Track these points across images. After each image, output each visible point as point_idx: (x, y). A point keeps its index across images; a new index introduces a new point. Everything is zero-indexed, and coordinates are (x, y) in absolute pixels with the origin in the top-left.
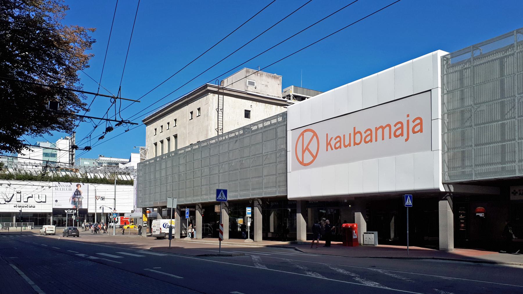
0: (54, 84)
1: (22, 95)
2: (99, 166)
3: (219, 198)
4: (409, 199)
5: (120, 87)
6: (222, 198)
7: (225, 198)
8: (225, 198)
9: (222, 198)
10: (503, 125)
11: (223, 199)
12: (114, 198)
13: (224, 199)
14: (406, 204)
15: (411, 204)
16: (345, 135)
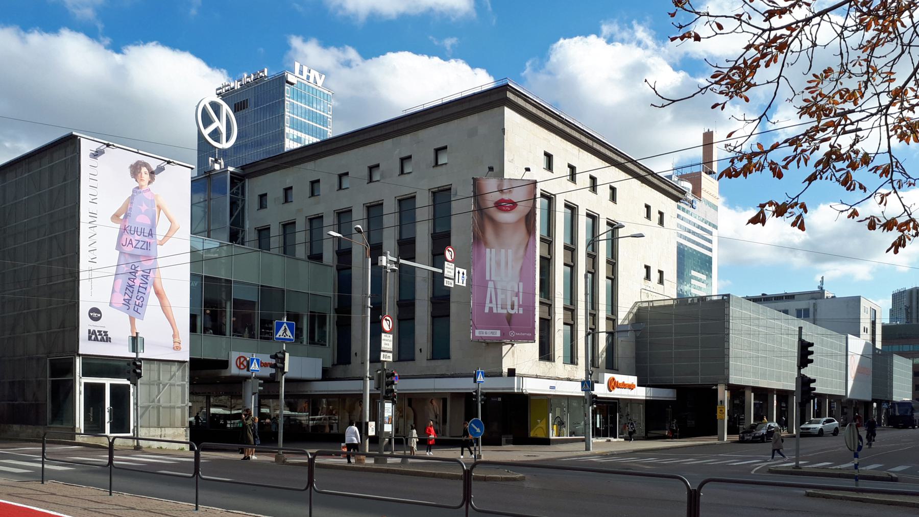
0: (915, 129)
1: (669, 408)
2: (825, 148)
3: (280, 336)
4: (285, 329)
5: (828, 44)
6: (285, 336)
7: (290, 336)
8: (290, 336)
9: (285, 336)
10: (65, 180)
11: (286, 337)
12: (169, 409)
13: (288, 337)
14: (277, 336)
15: (292, 338)
16: (802, 327)
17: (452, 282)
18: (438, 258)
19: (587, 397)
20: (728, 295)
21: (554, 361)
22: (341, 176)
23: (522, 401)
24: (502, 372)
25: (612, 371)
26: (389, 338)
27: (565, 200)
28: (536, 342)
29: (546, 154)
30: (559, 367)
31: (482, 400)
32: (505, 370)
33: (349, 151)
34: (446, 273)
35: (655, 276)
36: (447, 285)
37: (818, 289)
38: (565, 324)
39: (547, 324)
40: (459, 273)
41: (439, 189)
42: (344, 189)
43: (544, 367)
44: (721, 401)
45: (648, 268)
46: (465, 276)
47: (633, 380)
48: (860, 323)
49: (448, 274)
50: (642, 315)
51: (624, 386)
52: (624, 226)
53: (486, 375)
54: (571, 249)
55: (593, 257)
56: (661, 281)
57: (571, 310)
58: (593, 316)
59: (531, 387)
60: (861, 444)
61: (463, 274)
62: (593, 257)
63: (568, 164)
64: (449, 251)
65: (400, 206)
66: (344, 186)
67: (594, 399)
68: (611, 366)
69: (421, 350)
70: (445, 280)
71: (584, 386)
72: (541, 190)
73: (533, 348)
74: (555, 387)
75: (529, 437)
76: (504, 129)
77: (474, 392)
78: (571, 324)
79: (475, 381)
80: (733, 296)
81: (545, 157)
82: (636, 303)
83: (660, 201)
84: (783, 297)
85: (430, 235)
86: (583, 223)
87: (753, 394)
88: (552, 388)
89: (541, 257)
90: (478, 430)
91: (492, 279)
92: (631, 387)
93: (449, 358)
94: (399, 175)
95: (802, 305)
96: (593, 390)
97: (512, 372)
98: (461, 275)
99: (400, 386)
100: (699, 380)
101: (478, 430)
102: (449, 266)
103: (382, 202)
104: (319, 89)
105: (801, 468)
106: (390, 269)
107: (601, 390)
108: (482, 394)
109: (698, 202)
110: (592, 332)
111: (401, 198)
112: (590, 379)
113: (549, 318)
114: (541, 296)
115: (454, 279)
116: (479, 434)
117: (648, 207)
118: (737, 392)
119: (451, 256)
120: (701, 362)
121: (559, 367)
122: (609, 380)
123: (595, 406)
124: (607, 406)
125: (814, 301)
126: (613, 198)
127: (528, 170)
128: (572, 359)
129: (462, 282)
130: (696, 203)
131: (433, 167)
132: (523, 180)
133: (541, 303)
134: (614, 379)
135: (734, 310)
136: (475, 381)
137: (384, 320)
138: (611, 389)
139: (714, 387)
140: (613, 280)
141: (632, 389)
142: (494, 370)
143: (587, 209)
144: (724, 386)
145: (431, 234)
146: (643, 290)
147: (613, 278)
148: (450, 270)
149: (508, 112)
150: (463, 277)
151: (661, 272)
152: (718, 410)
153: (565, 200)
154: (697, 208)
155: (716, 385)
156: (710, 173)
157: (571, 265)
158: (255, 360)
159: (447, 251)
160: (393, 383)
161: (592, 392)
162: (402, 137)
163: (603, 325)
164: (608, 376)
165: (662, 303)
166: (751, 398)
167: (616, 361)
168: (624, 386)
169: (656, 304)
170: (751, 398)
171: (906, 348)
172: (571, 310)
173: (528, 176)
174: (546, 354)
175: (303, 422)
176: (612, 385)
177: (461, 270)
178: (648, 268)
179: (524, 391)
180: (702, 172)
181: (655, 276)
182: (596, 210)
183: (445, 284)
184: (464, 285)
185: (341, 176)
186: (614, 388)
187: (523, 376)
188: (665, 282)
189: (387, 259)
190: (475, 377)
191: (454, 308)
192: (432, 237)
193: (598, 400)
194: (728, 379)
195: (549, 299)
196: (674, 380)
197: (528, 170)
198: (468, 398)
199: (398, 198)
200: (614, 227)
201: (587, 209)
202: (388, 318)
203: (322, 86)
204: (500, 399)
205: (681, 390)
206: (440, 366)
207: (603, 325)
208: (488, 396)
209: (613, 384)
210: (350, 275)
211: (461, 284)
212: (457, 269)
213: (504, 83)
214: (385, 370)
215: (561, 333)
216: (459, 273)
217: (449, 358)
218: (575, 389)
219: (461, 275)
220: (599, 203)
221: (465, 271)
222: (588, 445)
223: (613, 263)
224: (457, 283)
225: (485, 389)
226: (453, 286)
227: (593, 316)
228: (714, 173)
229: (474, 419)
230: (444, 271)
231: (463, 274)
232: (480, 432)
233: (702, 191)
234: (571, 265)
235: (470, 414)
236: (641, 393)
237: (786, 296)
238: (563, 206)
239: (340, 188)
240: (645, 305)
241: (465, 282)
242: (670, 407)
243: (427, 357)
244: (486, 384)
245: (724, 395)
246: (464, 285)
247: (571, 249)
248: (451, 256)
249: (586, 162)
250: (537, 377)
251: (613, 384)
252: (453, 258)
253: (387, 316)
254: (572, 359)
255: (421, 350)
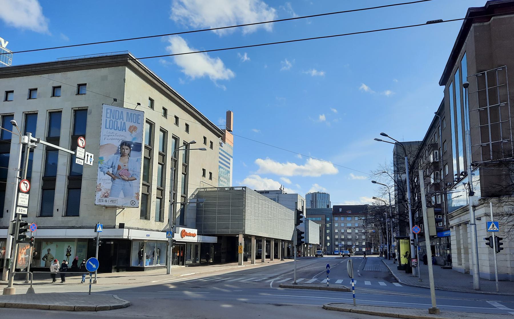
17: (83, 161)
18: (74, 146)
19: (169, 241)
20: (245, 187)
21: (149, 219)
22: (7, 93)
23: (127, 243)
24: (115, 226)
25: (183, 226)
26: (25, 197)
27: (160, 127)
28: (139, 207)
29: (150, 99)
30: (152, 223)
31: (100, 244)
32: (117, 224)
33: (16, 78)
34: (78, 155)
35: (207, 175)
36: (78, 163)
37: (279, 190)
38: (157, 198)
39: (146, 197)
40: (88, 155)
41: (79, 109)
42: (9, 101)
43: (143, 223)
44: (241, 244)
45: (204, 170)
46: (92, 158)
47: (195, 231)
48: (481, 188)
49: (80, 155)
50: (198, 196)
51: (190, 235)
52: (196, 143)
53: (104, 228)
54: (163, 155)
55: (175, 161)
56: (211, 178)
57: (161, 190)
58: (174, 196)
59: (134, 235)
60: (329, 270)
61: (91, 157)
62: (175, 161)
63: (163, 107)
64: (81, 140)
65: (50, 116)
66: (9, 99)
67: (174, 243)
68: (182, 223)
69: (58, 210)
70: (77, 159)
71: (168, 235)
72: (146, 118)
73: (137, 211)
74: (149, 235)
75: (130, 266)
76: (125, 79)
77: (94, 238)
78: (161, 199)
79: (96, 231)
80: (247, 188)
81: (150, 101)
82: (198, 189)
83: (211, 137)
84: (264, 192)
85: (71, 137)
86: (170, 142)
87: (255, 240)
88: (148, 236)
89: (145, 157)
90: (94, 266)
91: (94, 277)
92: (194, 236)
93: (78, 216)
94: (51, 97)
95: (274, 196)
96: (174, 237)
97: (122, 226)
98: (89, 157)
99: (32, 233)
100: (229, 231)
101: (94, 266)
102: (80, 150)
103: (37, 112)
104: (3, 49)
105: (297, 284)
106: (31, 146)
107: (177, 237)
108: (100, 239)
109: (224, 144)
110: (173, 204)
111: (51, 111)
112: (172, 231)
113: (148, 194)
114: (143, 180)
115: (84, 160)
116: (95, 269)
117: (205, 138)
118: (248, 238)
119: (83, 144)
120: (216, 223)
121: (152, 223)
122: (182, 230)
123: (174, 247)
124: (179, 247)
125: (278, 195)
126: (187, 130)
127: (139, 104)
128: (160, 219)
129: (90, 162)
130: (223, 144)
131: (76, 95)
132: (136, 110)
133: (143, 184)
134: (185, 231)
135: (248, 195)
136: (96, 231)
137: (22, 183)
138: (183, 237)
139: (237, 236)
140: (185, 175)
141: (194, 237)
142: (110, 224)
143: (173, 134)
144: (242, 235)
145: (72, 136)
146: (201, 182)
147: (186, 174)
148: (81, 153)
149: (127, 69)
150: (91, 159)
151: (211, 173)
152: (239, 248)
153: (160, 127)
154: (223, 147)
155: (238, 235)
156: (230, 131)
157: (163, 165)
158: (100, 225)
159: (79, 140)
160: (25, 230)
161: (173, 238)
162: (55, 74)
163: (179, 199)
164: (181, 229)
165: (211, 190)
166: (254, 242)
167: (185, 220)
168: (190, 235)
169: (208, 190)
170: (254, 242)
171: (314, 219)
172: (161, 190)
173: (139, 108)
174: (145, 215)
175: (418, 160)
176: (183, 234)
177: (90, 155)
178: (204, 170)
179: (129, 238)
180: (226, 130)
181: (207, 175)
182: (178, 135)
183: (77, 162)
184: (92, 164)
185: (7, 93)
186: (184, 236)
187: (129, 229)
188: (213, 179)
189: (29, 138)
190: (96, 228)
191: (84, 183)
192: (72, 137)
193: (176, 243)
194: (244, 231)
195: (148, 182)
196: (217, 231)
197: (139, 104)
198: (91, 242)
199: (49, 111)
200: (187, 145)
201: (173, 134)
202: (26, 182)
203: (6, 47)
204: (112, 243)
205: (220, 237)
206: (72, 220)
207: (179, 199)
208: (104, 241)
209: (184, 234)
210: (8, 158)
211: (89, 163)
212: (87, 153)
213: (126, 53)
214: (20, 220)
215: (155, 203)
216: (88, 155)
217: (78, 216)
218: (163, 237)
219: (89, 157)
220: (180, 131)
221: (93, 155)
222: (168, 271)
223: (186, 166)
224: (86, 162)
225: (103, 236)
226: (82, 164)
227: (174, 196)
228: (231, 131)
229: (92, 258)
230: (76, 153)
231: (91, 157)
232: (95, 267)
233: (226, 139)
234: (163, 165)
235: (91, 254)
236: (195, 239)
237: (265, 192)
238: (159, 129)
239: (6, 100)
240: (203, 190)
241: (92, 163)
242: (213, 246)
243: (62, 215)
244: (103, 233)
245: (241, 240)
246: (92, 164)
247: (163, 155)
248: (83, 144)
249: (174, 109)
250: (138, 229)
251: (184, 234)
252: (84, 145)
253: (25, 180)
254: (160, 219)
255: (58, 210)
